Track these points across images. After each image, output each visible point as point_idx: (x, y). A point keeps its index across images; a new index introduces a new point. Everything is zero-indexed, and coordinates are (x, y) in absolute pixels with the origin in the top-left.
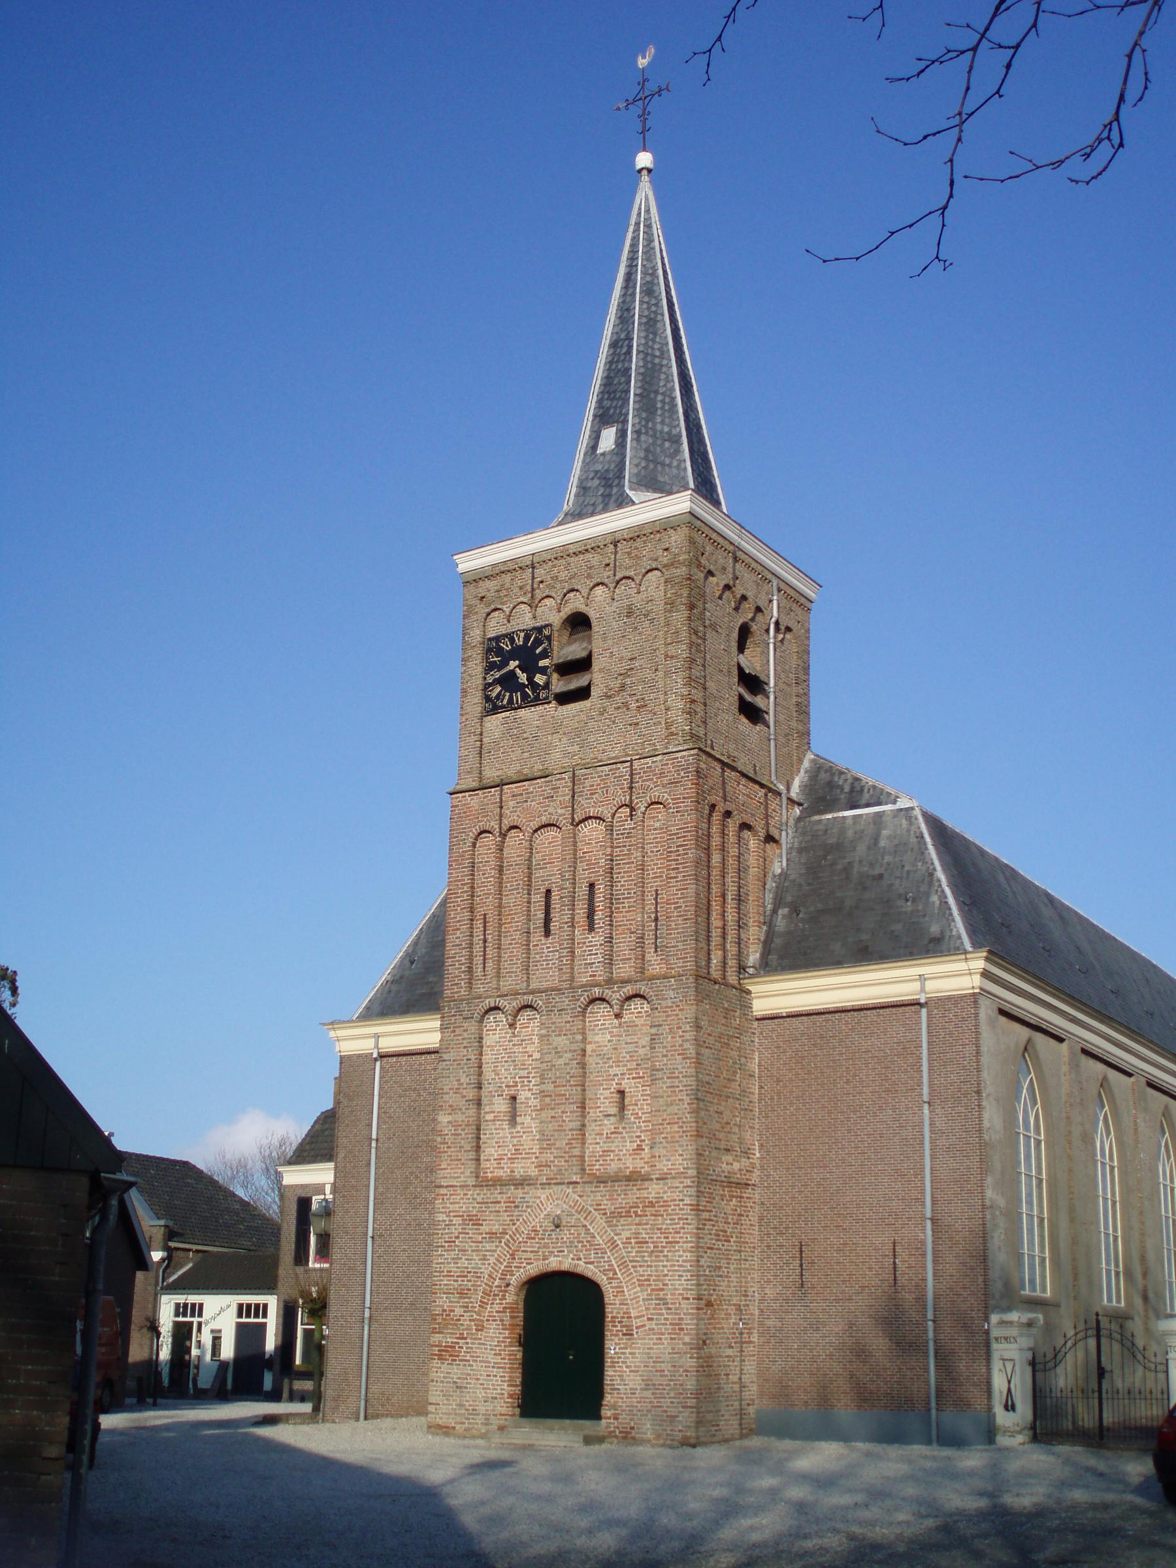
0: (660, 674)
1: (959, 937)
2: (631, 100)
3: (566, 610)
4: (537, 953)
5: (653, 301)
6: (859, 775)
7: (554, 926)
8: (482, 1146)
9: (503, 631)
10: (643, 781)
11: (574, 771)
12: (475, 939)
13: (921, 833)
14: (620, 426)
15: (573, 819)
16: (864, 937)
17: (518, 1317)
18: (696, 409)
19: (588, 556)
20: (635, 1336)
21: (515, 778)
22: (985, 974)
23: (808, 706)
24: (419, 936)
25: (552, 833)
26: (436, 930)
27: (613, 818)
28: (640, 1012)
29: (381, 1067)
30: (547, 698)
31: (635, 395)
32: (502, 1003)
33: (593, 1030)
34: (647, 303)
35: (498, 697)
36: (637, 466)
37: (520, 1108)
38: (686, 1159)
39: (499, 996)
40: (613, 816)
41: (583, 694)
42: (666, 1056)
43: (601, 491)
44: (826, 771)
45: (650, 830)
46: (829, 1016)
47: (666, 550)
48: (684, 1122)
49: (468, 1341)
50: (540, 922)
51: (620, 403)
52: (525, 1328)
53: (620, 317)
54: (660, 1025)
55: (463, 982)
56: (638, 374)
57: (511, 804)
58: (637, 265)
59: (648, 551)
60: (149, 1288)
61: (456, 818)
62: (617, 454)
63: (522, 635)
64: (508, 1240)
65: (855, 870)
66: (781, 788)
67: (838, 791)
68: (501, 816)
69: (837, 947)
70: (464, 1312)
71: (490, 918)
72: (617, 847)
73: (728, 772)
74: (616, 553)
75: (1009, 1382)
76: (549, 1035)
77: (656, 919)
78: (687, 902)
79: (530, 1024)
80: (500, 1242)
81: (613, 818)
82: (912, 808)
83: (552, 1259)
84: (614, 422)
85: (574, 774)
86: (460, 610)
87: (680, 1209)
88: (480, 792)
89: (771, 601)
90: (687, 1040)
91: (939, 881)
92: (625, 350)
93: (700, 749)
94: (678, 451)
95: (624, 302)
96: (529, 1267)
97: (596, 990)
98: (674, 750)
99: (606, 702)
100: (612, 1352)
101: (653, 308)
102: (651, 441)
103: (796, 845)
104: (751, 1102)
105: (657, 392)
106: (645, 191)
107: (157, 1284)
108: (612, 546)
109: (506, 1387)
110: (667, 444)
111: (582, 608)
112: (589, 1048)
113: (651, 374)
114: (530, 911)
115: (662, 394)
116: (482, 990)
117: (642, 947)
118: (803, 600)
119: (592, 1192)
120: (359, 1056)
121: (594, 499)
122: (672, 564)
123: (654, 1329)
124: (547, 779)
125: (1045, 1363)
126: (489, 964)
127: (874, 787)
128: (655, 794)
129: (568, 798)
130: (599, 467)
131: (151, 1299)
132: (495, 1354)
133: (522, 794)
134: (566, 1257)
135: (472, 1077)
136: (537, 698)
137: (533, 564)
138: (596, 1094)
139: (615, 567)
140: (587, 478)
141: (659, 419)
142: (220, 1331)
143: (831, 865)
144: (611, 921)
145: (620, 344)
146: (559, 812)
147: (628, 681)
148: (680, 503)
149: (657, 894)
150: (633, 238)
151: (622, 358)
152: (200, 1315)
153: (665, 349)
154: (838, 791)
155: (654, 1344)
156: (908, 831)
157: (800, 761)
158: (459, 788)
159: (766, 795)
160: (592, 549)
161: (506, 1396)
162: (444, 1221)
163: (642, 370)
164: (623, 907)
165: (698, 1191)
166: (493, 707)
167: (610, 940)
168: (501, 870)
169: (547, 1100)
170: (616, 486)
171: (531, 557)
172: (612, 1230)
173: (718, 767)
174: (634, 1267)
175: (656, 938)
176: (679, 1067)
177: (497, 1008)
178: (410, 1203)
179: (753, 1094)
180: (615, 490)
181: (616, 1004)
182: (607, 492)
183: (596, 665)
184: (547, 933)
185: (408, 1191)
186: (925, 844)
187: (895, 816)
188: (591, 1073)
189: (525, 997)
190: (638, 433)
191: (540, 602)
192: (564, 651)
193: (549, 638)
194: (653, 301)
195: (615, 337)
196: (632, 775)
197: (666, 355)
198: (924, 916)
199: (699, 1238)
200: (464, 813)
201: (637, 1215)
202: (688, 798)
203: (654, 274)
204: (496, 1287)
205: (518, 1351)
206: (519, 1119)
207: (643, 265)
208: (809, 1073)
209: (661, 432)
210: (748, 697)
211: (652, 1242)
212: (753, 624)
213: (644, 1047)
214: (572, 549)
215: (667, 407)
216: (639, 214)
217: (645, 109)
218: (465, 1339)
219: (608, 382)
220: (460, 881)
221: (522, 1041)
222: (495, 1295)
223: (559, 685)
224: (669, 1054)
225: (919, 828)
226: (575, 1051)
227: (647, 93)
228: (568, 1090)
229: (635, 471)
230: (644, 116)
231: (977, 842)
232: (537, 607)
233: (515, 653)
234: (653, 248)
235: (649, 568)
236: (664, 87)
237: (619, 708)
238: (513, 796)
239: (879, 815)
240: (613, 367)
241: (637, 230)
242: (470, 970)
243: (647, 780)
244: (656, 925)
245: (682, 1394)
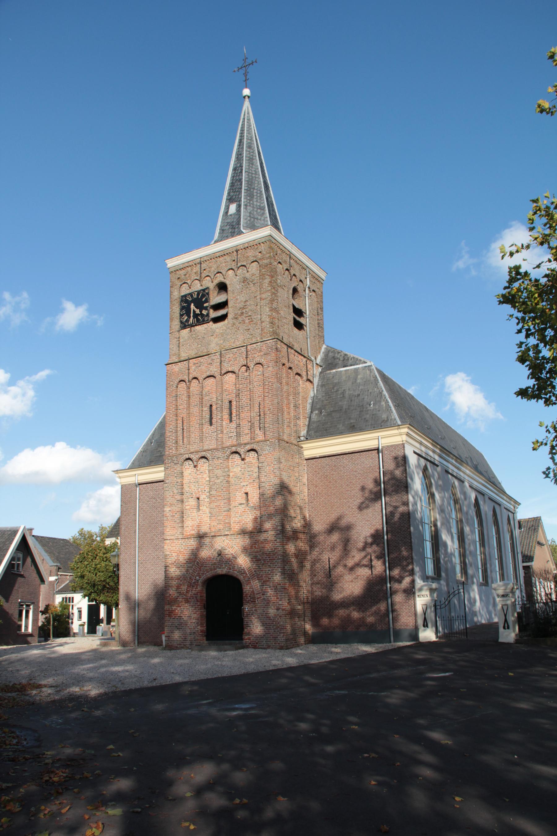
0: (259, 307)
1: (395, 419)
2: (240, 68)
3: (216, 281)
4: (207, 433)
5: (252, 151)
6: (347, 353)
7: (214, 420)
8: (185, 520)
9: (188, 292)
10: (252, 354)
11: (221, 352)
12: (179, 429)
13: (376, 376)
14: (238, 203)
15: (221, 373)
16: (352, 421)
17: (203, 596)
18: (271, 197)
19: (226, 257)
20: (257, 602)
21: (195, 356)
22: (408, 434)
23: (323, 325)
24: (155, 431)
25: (212, 379)
26: (162, 426)
27: (239, 371)
28: (254, 457)
29: (139, 489)
30: (208, 320)
31: (245, 190)
32: (192, 456)
33: (233, 466)
34: (249, 151)
36: (246, 219)
37: (201, 502)
38: (277, 522)
39: (190, 453)
40: (239, 370)
41: (223, 318)
42: (266, 476)
43: (231, 230)
44: (332, 352)
45: (255, 376)
46: (338, 457)
47: (260, 252)
48: (275, 505)
49: (182, 608)
50: (208, 420)
51: (238, 193)
52: (207, 601)
53: (237, 158)
54: (263, 462)
55: (174, 448)
56: (245, 181)
57: (193, 368)
58: (244, 136)
59: (251, 253)
60: (51, 592)
61: (169, 376)
62: (237, 215)
63: (196, 293)
64: (198, 562)
65: (347, 393)
66: (313, 358)
67: (338, 360)
68: (189, 373)
69: (340, 426)
70: (180, 595)
71: (185, 419)
72: (241, 384)
73: (289, 350)
74: (237, 255)
76: (213, 470)
77: (260, 415)
78: (273, 407)
79: (204, 466)
80: (194, 563)
81: (239, 371)
82: (371, 366)
83: (218, 569)
84: (235, 202)
85: (221, 353)
86: (169, 284)
87: (275, 545)
88: (179, 363)
89: (306, 278)
90: (276, 469)
91: (385, 395)
92: (239, 171)
93: (277, 339)
94: (263, 214)
95: (239, 151)
96: (207, 573)
97: (234, 448)
98: (266, 340)
99: (235, 321)
100: (247, 610)
101: (252, 154)
102: (252, 209)
103: (320, 384)
104: (304, 496)
105: (254, 189)
106: (247, 104)
107: (54, 590)
108: (235, 252)
109: (199, 628)
110: (259, 211)
111: (223, 280)
112: (231, 474)
113: (250, 183)
114: (203, 415)
115: (256, 189)
116: (182, 451)
118: (319, 279)
119: (235, 538)
120: (129, 484)
121: (227, 234)
122: (263, 258)
123: (265, 599)
124: (209, 356)
125: (441, 606)
126: (185, 440)
127: (354, 358)
128: (258, 360)
129: (218, 364)
130: (229, 221)
131: (52, 596)
132: (194, 613)
133: (198, 363)
134: (224, 568)
135: (179, 490)
136: (204, 320)
137: (200, 262)
138: (235, 495)
139: (237, 261)
140: (224, 226)
141: (255, 200)
142: (81, 608)
143: (336, 391)
144: (239, 417)
145: (237, 169)
146: (214, 369)
147: (244, 311)
148: (267, 231)
150: (242, 125)
151: (238, 174)
152: (73, 602)
153: (257, 171)
154: (338, 360)
155: (265, 605)
156: (370, 375)
157: (320, 348)
158: (170, 362)
159: (306, 361)
160: (227, 254)
161: (199, 631)
162: (169, 555)
163: (247, 179)
164: (245, 411)
165: (283, 536)
166: (184, 326)
167: (238, 426)
168: (189, 397)
169: (213, 498)
170: (237, 228)
171: (199, 259)
173: (285, 347)
175: (260, 424)
176: (273, 480)
177: (189, 459)
178: (154, 548)
179: (305, 492)
180: (236, 230)
181: (243, 454)
182: (233, 231)
183: (230, 304)
184: (211, 424)
185: (153, 543)
186: (378, 380)
187: (363, 370)
188: (232, 485)
189: (202, 453)
190: (246, 205)
191: (204, 278)
192: (215, 300)
193: (208, 294)
194: (252, 151)
195: (235, 166)
196: (247, 352)
197: (257, 173)
198: (379, 411)
199: (284, 557)
201: (255, 548)
202: (273, 360)
203: (252, 139)
204: (193, 583)
205: (204, 611)
206: (201, 508)
207: (247, 136)
208: (330, 482)
209: (256, 205)
210: (297, 318)
211: (263, 560)
212: (298, 287)
213: (256, 472)
214: (218, 254)
215: (258, 195)
216: (245, 115)
217: (246, 71)
218: (180, 607)
219: (232, 185)
220: (171, 403)
221: (201, 473)
222: (193, 587)
223: (213, 314)
224: (268, 475)
225: (375, 374)
226: (225, 476)
227: (247, 64)
228: (222, 494)
229: (245, 221)
230: (245, 74)
231: (397, 383)
232: (202, 281)
233: (194, 301)
234: (251, 129)
235: (252, 261)
236: (254, 61)
237: (240, 323)
238: (194, 364)
239: (356, 370)
240: (235, 178)
241: (244, 121)
242: (177, 442)
243: (254, 354)
244: (260, 418)
245: (279, 627)
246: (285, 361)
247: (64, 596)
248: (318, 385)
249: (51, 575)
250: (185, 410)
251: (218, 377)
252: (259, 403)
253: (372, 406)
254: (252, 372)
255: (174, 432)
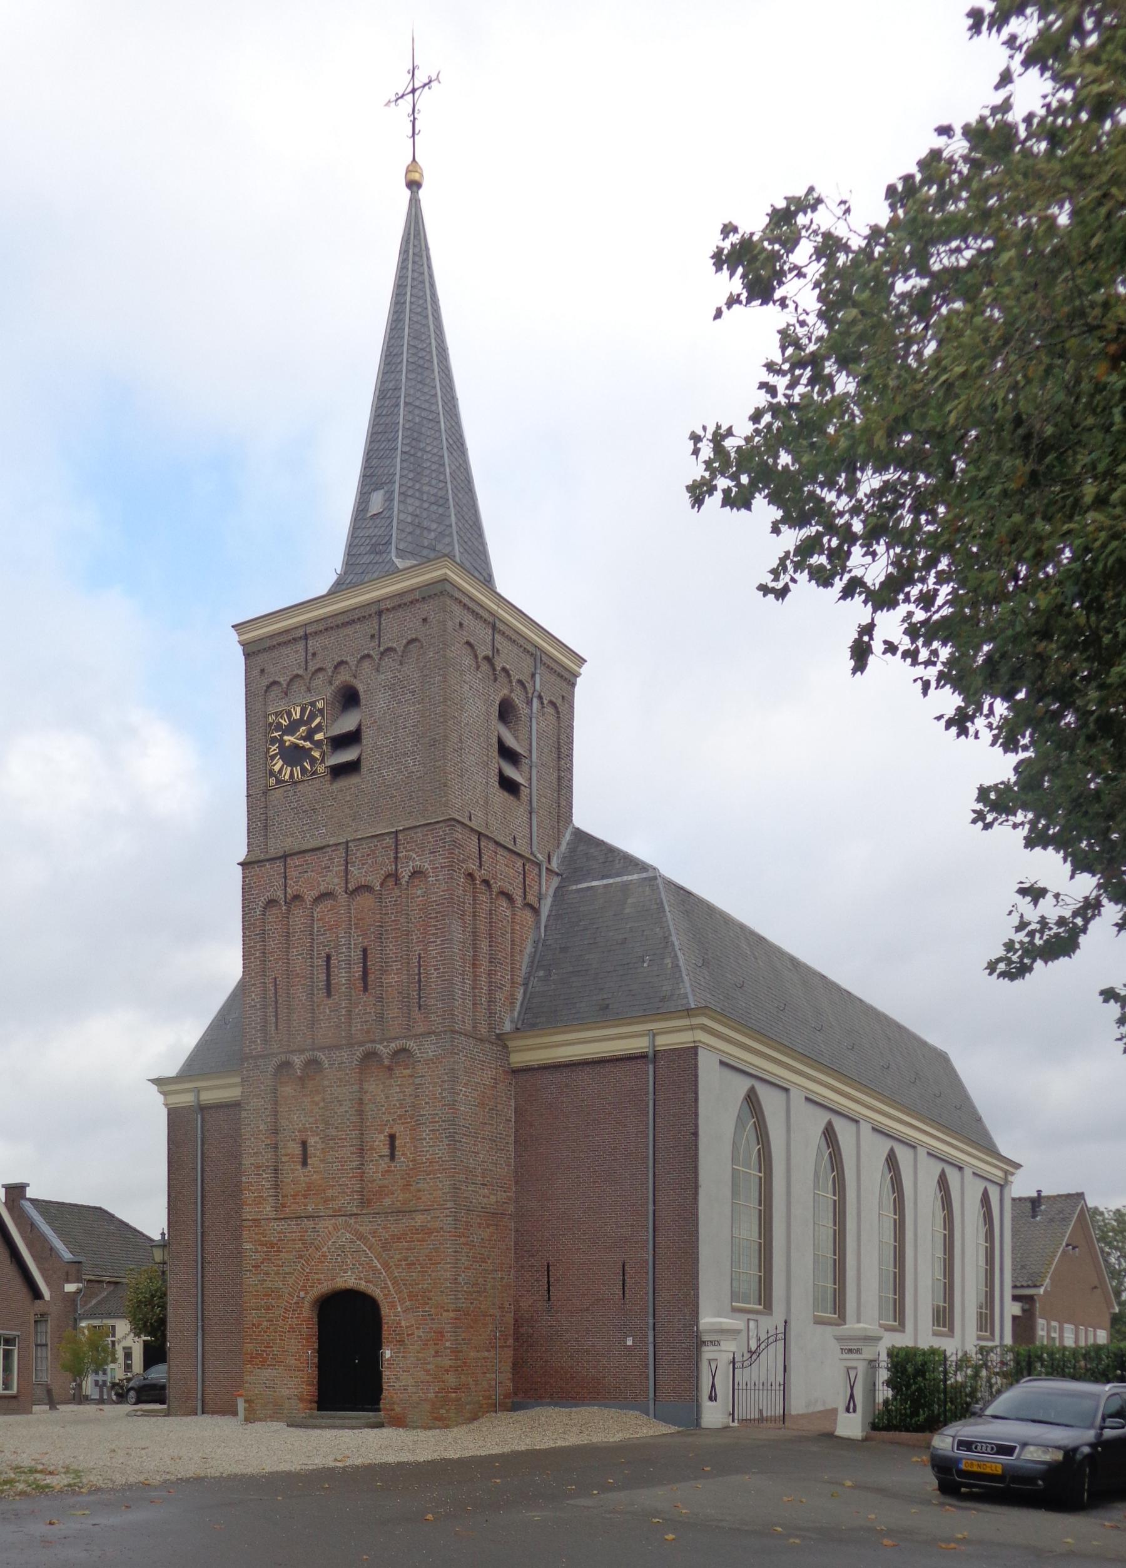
15: (347, 888)
35: (280, 771)
41: (351, 768)
50: (322, 985)
75: (852, 1388)
90: (445, 1089)
91: (673, 945)
117: (409, 1006)
119: (370, 1222)
137: (306, 635)
146: (333, 881)
149: (420, 958)
152: (114, 1336)
172: (387, 1254)
174: (404, 1284)
175: (420, 998)
181: (387, 1058)
196: (397, 845)
200: (255, 883)
204: (295, 1303)
206: (309, 1161)
228: (348, 1135)
239: (626, 886)
246: (472, 866)
247: (96, 1322)
248: (549, 916)
249: (68, 1281)
250: (280, 964)
251: (343, 898)
252: (419, 954)
253: (645, 965)
254: (407, 889)
255: (258, 1007)
